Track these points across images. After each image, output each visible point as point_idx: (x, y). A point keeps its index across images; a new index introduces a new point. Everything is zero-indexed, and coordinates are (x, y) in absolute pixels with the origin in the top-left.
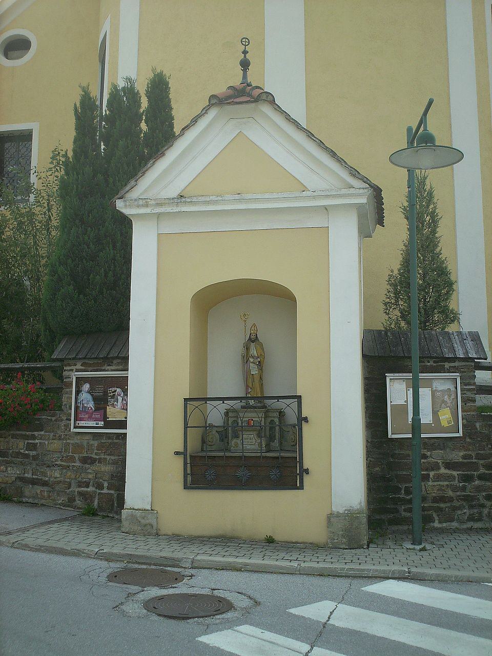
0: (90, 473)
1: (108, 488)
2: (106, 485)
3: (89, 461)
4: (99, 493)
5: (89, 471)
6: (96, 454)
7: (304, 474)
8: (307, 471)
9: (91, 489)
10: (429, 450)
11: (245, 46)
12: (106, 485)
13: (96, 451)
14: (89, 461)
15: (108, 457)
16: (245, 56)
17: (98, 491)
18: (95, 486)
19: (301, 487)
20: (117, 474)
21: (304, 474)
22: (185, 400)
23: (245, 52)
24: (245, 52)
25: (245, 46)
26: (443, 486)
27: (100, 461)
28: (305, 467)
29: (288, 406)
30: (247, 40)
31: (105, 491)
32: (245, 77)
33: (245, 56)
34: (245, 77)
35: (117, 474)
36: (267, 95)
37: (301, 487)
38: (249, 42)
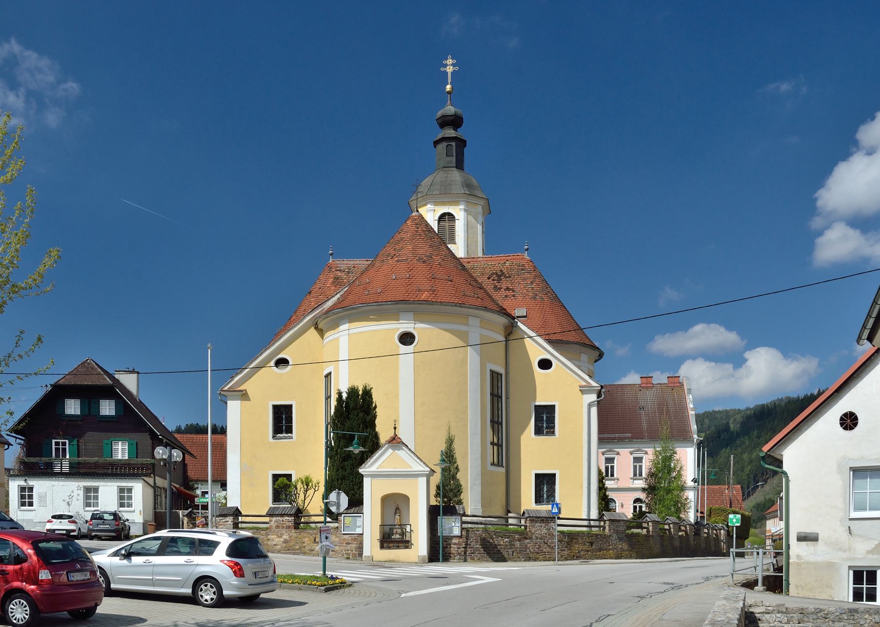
2: (354, 550)
9: (349, 552)
12: (354, 550)
19: (411, 548)
37: (411, 548)
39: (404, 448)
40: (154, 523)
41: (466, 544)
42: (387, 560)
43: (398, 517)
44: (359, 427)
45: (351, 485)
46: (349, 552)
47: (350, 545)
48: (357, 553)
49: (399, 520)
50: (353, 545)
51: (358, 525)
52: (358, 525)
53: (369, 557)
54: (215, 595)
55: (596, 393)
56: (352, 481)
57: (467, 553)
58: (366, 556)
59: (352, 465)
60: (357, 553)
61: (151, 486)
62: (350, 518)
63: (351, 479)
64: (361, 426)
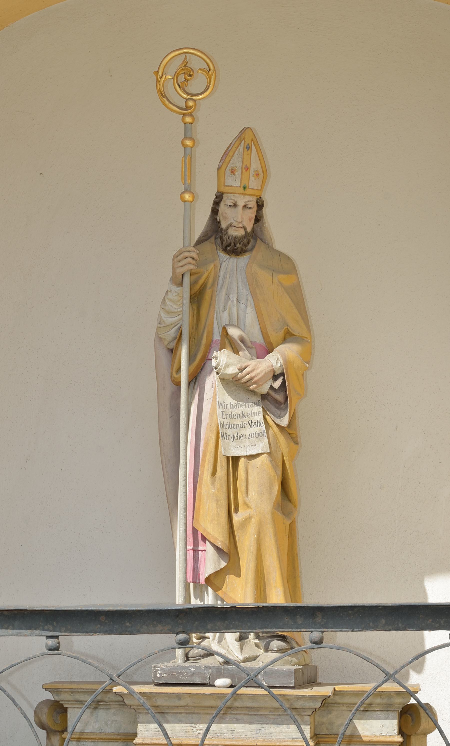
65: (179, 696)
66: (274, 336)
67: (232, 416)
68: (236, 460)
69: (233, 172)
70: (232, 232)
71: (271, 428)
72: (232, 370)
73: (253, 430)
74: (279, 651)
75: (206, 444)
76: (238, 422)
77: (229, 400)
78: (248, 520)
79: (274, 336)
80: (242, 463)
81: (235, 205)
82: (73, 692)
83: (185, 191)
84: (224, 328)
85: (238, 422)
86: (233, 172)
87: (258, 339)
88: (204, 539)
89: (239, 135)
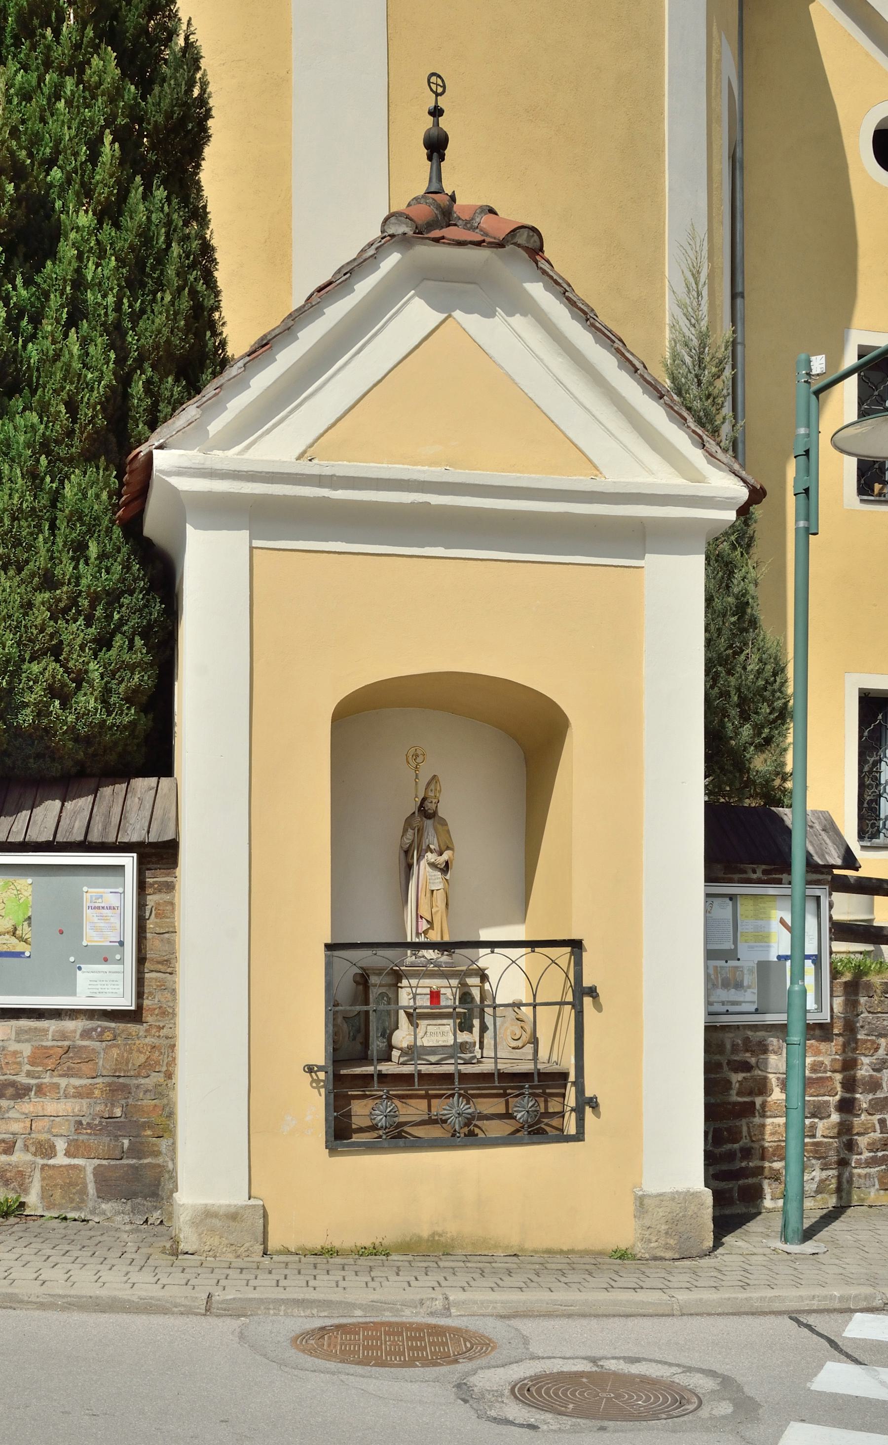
0: (17, 1120)
1: (68, 1154)
2: (61, 1145)
3: (10, 1091)
4: (43, 1167)
5: (12, 1114)
6: (29, 1074)
7: (588, 1110)
8: (593, 1103)
9: (19, 1157)
10: (753, 1052)
11: (437, 95)
12: (61, 1145)
13: (28, 1067)
14: (10, 1091)
15: (63, 1082)
16: (436, 124)
17: (41, 1161)
18: (33, 1149)
19: (579, 1136)
20: (93, 1119)
21: (588, 1110)
22: (328, 947)
23: (436, 112)
24: (436, 112)
25: (437, 95)
26: (779, 1126)
27: (40, 1090)
28: (588, 1093)
29: (513, 962)
30: (439, 82)
31: (60, 1160)
32: (437, 175)
33: (436, 124)
34: (437, 175)
35: (93, 1119)
36: (531, 233)
37: (579, 1136)
38: (429, 82)
39: (537, 290)
40: (147, 880)
41: (850, 1085)
42: (389, 1236)
43: (436, 880)
44: (94, 157)
45: (41, 615)
46: (19, 1157)
47: (27, 1106)
48: (88, 1165)
49: (440, 897)
50: (52, 1107)
51: (91, 937)
52: (91, 937)
53: (234, 1216)
54: (860, 357)
55: (703, 547)
56: (49, 582)
57: (862, 1142)
58: (208, 1214)
59: (45, 447)
60: (88, 1165)
61: (472, 986)
62: (25, 883)
63: (41, 561)
64: (109, 149)
65: (418, 970)
66: (443, 848)
67: (432, 876)
68: (433, 891)
69: (431, 791)
70: (429, 811)
71: (90, 798)
72: (433, 860)
73: (438, 881)
74: (447, 955)
75: (422, 885)
76: (433, 878)
77: (430, 870)
78: (437, 911)
79: (443, 848)
80: (435, 892)
81: (431, 802)
82: (373, 969)
83: (416, 797)
84: (429, 846)
85: (433, 878)
86: (431, 791)
87: (437, 849)
88: (421, 917)
89: (844, 956)
